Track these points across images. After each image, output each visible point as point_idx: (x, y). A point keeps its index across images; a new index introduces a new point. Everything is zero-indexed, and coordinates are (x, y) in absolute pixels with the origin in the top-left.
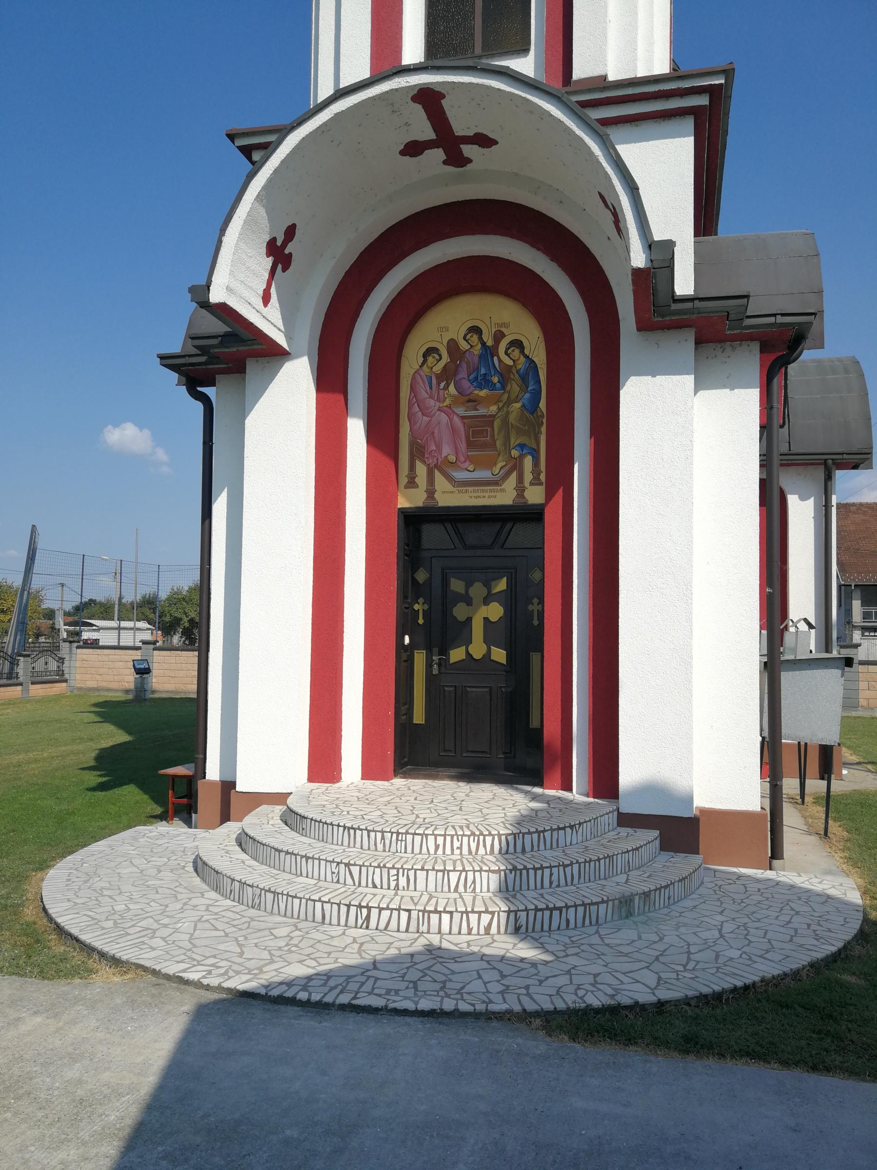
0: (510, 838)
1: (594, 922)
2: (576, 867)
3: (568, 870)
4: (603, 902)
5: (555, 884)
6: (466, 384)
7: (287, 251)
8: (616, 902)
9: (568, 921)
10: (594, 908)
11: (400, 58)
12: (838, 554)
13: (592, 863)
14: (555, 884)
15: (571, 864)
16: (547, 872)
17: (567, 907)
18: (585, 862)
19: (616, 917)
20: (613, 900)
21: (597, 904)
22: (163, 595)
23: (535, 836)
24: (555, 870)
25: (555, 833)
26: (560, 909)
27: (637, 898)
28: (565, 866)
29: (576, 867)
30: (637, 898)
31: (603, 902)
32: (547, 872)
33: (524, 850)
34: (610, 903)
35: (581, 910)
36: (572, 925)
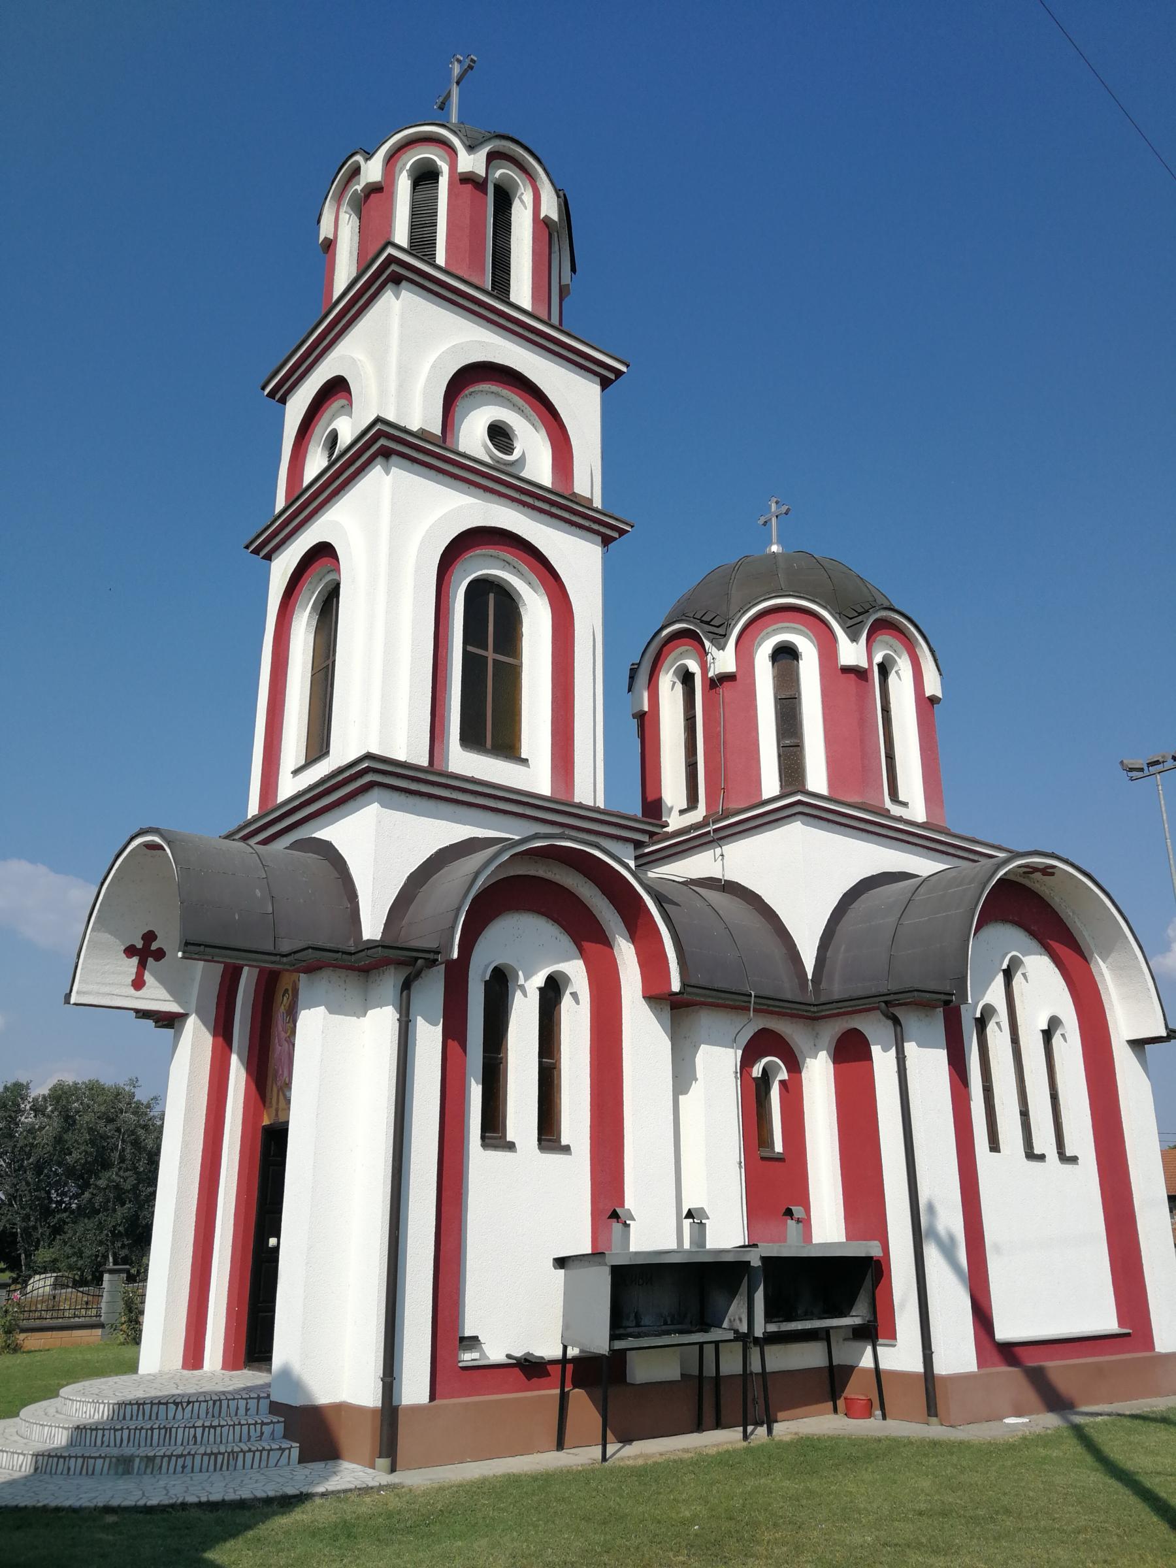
0: (116, 1407)
1: (90, 1472)
2: (126, 1432)
3: (118, 1434)
4: (100, 1457)
5: (106, 1443)
6: (444, 168)
7: (542, 216)
8: (114, 1460)
9: (69, 1469)
10: (91, 1461)
11: (761, 795)
12: (514, 1480)
13: (143, 1432)
14: (106, 1443)
15: (122, 1429)
16: (100, 1432)
17: (70, 1457)
18: (136, 1429)
19: (112, 1472)
20: (111, 1458)
21: (95, 1458)
22: (40, 1090)
23: (135, 1407)
24: (107, 1432)
25: (155, 1408)
26: (65, 1458)
27: (137, 1460)
28: (116, 1430)
29: (126, 1432)
30: (137, 1460)
31: (100, 1457)
32: (100, 1432)
33: (124, 1418)
34: (107, 1460)
35: (80, 1461)
36: (72, 1472)
